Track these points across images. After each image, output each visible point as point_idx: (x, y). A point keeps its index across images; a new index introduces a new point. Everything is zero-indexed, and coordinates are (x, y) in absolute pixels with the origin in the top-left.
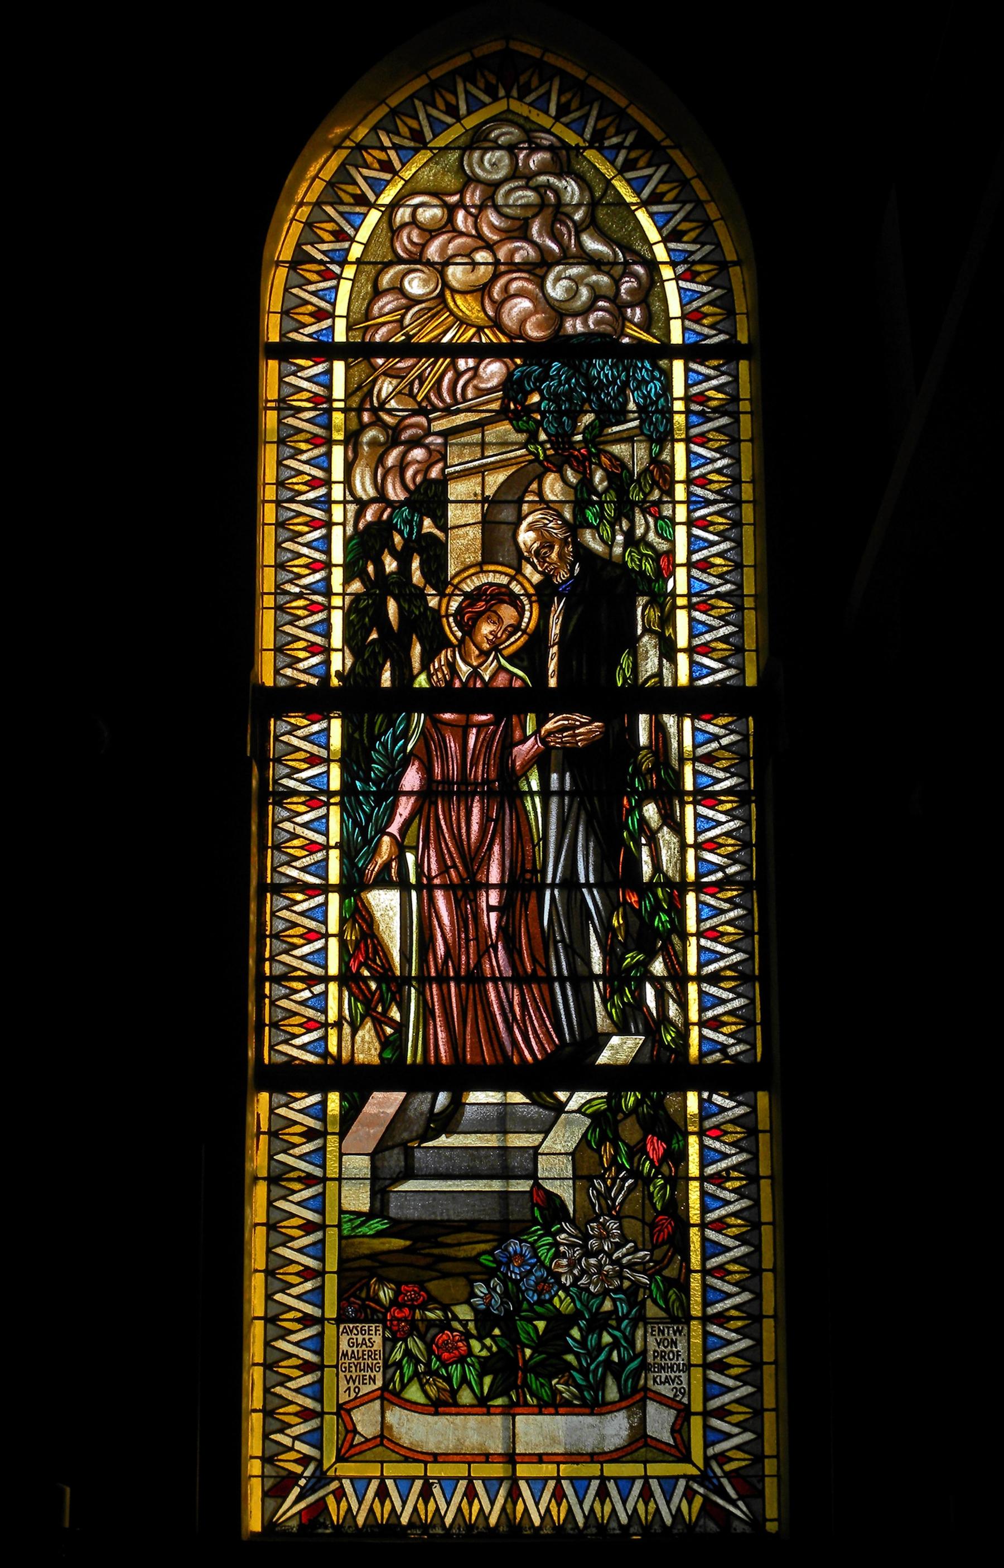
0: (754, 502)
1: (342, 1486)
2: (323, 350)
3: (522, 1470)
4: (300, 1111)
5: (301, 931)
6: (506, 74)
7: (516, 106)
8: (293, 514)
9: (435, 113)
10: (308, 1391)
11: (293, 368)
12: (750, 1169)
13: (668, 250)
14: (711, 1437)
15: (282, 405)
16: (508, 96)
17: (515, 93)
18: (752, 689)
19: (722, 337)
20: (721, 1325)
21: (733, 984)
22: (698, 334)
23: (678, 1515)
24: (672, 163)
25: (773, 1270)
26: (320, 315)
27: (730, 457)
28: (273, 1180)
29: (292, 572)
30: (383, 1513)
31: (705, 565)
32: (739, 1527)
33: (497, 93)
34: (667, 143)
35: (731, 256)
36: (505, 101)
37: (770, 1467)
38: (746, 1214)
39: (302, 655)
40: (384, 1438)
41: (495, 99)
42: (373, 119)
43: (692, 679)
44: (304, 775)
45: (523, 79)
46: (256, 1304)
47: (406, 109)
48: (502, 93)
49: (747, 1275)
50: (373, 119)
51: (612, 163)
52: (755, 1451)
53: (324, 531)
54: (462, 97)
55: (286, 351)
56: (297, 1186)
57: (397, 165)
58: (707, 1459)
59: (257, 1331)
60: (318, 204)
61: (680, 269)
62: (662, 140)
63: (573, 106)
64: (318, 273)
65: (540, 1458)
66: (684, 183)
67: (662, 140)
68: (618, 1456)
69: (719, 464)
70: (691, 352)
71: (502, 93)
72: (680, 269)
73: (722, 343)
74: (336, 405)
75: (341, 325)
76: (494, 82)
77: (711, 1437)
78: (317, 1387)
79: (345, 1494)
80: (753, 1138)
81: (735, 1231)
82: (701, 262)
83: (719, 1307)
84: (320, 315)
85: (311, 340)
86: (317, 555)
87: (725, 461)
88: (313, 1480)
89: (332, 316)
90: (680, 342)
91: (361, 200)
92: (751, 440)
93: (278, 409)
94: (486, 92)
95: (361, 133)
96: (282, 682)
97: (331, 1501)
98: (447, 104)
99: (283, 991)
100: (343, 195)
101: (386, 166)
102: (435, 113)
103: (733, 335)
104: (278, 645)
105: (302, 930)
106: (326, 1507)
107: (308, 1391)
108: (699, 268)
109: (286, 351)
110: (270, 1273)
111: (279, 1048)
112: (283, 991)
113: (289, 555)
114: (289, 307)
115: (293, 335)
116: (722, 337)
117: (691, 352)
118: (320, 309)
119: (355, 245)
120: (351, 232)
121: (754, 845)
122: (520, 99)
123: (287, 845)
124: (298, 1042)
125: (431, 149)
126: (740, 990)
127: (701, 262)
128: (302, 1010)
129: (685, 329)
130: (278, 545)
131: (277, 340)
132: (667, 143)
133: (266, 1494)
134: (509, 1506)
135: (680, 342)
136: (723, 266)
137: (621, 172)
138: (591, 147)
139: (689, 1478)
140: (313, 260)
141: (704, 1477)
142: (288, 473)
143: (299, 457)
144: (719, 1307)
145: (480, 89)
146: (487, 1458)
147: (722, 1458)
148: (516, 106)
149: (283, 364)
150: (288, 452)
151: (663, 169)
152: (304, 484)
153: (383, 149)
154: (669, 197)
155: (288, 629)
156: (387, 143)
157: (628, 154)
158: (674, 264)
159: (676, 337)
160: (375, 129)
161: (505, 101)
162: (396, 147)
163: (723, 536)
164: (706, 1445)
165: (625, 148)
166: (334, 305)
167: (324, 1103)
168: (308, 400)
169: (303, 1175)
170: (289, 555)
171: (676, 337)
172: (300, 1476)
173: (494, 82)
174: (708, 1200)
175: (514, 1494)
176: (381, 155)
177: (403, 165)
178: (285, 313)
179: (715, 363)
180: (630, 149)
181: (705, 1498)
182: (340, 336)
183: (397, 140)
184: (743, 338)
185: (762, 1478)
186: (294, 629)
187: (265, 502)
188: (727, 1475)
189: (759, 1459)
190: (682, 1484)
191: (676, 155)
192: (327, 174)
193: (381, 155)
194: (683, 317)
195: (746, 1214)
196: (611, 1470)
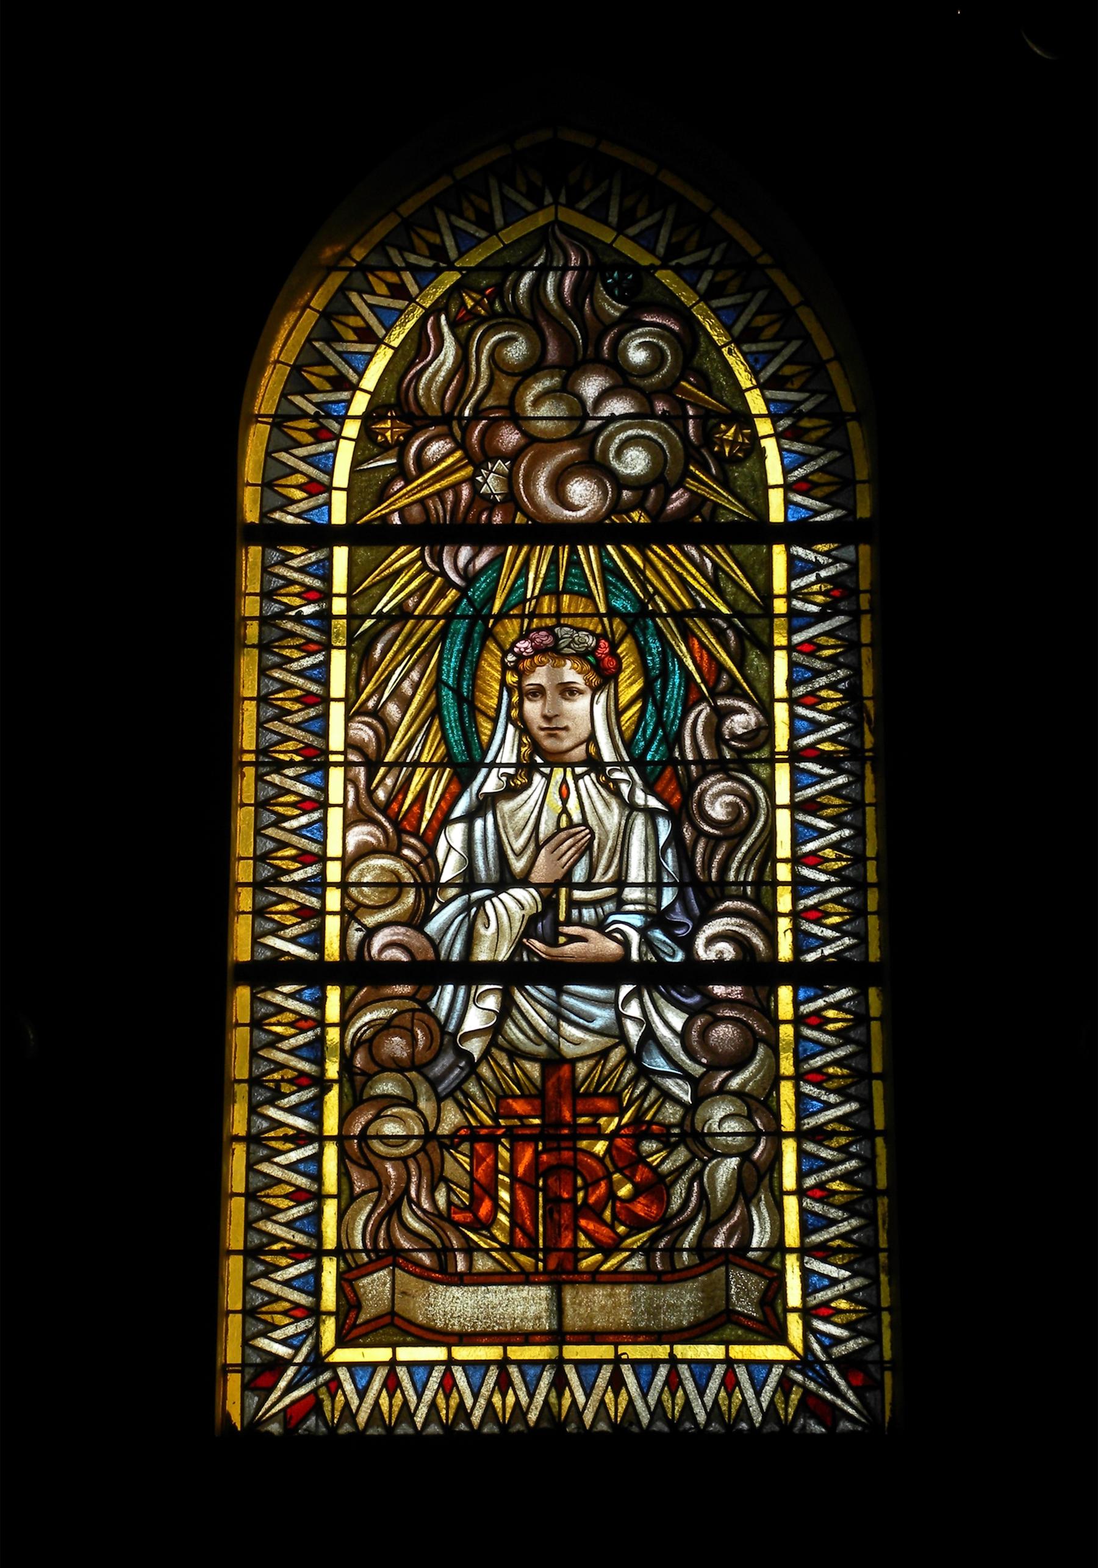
1: (336, 1378)
2: (321, 536)
3: (573, 1352)
5: (289, 1017)
7: (568, 216)
9: (460, 223)
10: (304, 1110)
11: (261, 1327)
13: (767, 402)
15: (261, 759)
16: (556, 203)
17: (563, 199)
19: (837, 513)
24: (773, 288)
27: (864, 1275)
29: (273, 920)
31: (812, 647)
32: (845, 1426)
34: (765, 259)
35: (848, 406)
36: (552, 209)
41: (540, 206)
42: (380, 232)
43: (798, 949)
44: (294, 824)
46: (235, 1236)
47: (425, 219)
48: (548, 199)
50: (380, 232)
51: (693, 287)
53: (310, 1206)
54: (496, 202)
55: (272, 535)
56: (283, 1261)
57: (413, 289)
59: (236, 1207)
61: (785, 423)
62: (759, 256)
63: (640, 213)
64: (310, 432)
67: (759, 256)
68: (695, 1334)
71: (548, 199)
72: (785, 423)
73: (835, 520)
74: (333, 758)
75: (339, 501)
76: (539, 183)
82: (811, 414)
85: (301, 521)
87: (858, 1282)
90: (781, 519)
91: (366, 335)
93: (256, 764)
94: (528, 196)
96: (263, 955)
97: (324, 1395)
98: (478, 211)
99: (261, 1268)
101: (398, 291)
102: (460, 223)
103: (852, 511)
104: (262, 745)
105: (290, 1017)
107: (304, 1053)
108: (805, 423)
109: (272, 535)
110: (250, 1196)
111: (260, 1167)
112: (261, 1268)
114: (273, 477)
115: (277, 515)
116: (837, 513)
117: (795, 533)
118: (312, 480)
122: (571, 205)
123: (277, 748)
124: (295, 666)
125: (460, 270)
127: (811, 414)
128: (294, 839)
129: (787, 502)
130: (260, 725)
132: (765, 259)
133: (245, 1387)
134: (553, 1399)
135: (781, 519)
136: (837, 419)
137: (705, 297)
138: (664, 266)
139: (788, 1364)
140: (305, 415)
142: (264, 1067)
143: (290, 563)
145: (521, 193)
146: (526, 1338)
148: (568, 216)
149: (268, 551)
151: (761, 295)
153: (397, 270)
154: (769, 333)
155: (276, 725)
156: (399, 262)
157: (713, 277)
158: (774, 418)
159: (776, 514)
161: (552, 209)
162: (414, 269)
165: (711, 267)
166: (331, 474)
168: (296, 752)
169: (291, 1132)
170: (275, 738)
172: (289, 1362)
173: (539, 183)
175: (560, 1383)
176: (392, 278)
177: (421, 289)
178: (261, 805)
180: (717, 268)
182: (339, 517)
183: (413, 259)
184: (864, 511)
186: (281, 833)
188: (838, 1362)
190: (777, 1371)
191: (778, 277)
193: (392, 278)
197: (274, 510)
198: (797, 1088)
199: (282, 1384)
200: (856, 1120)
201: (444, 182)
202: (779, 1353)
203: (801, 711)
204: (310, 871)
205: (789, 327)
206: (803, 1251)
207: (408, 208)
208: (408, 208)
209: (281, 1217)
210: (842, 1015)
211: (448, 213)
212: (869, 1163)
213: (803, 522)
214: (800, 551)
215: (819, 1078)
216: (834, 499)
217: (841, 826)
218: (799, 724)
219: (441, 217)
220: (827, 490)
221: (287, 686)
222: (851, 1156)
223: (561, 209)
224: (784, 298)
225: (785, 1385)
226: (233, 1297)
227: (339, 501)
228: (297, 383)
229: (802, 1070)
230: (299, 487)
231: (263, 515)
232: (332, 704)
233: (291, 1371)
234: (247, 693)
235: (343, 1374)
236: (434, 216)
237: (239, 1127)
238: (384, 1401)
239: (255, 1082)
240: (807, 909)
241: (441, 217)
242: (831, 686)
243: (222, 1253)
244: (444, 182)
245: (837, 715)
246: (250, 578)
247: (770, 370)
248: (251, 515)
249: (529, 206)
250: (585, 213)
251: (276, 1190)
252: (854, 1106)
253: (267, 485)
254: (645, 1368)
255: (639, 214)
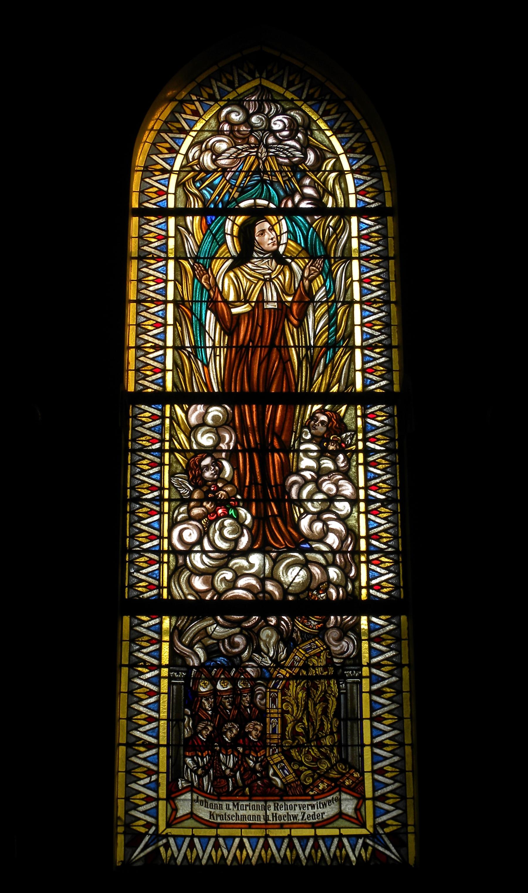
0: (412, 771)
1: (168, 841)
2: (163, 212)
4: (162, 159)
6: (261, 65)
7: (266, 83)
8: (139, 482)
12: (385, 298)
14: (375, 733)
17: (264, 75)
18: (396, 393)
19: (376, 204)
20: (378, 643)
21: (384, 454)
22: (366, 202)
23: (359, 858)
25: (409, 665)
26: (160, 193)
27: (395, 650)
28: (129, 745)
29: (141, 420)
30: (192, 857)
31: (368, 237)
33: (255, 75)
37: (411, 829)
38: (391, 531)
39: (152, 283)
40: (192, 815)
41: (254, 78)
42: (190, 88)
43: (364, 386)
45: (269, 68)
48: (257, 75)
49: (398, 800)
50: (190, 88)
52: (401, 819)
55: (142, 212)
57: (201, 112)
58: (375, 826)
60: (159, 131)
65: (282, 826)
66: (356, 122)
69: (384, 478)
70: (362, 212)
71: (257, 75)
75: (171, 198)
77: (375, 733)
78: (154, 811)
79: (170, 846)
80: (402, 748)
81: (379, 373)
83: (379, 712)
84: (160, 193)
86: (161, 276)
88: (154, 836)
89: (167, 193)
91: (182, 131)
92: (413, 798)
95: (184, 94)
97: (162, 849)
100: (174, 128)
101: (196, 113)
103: (384, 203)
106: (159, 851)
109: (142, 212)
111: (133, 706)
113: (142, 342)
119: (179, 155)
120: (177, 148)
121: (397, 440)
122: (267, 79)
126: (385, 353)
129: (357, 199)
131: (137, 206)
133: (126, 845)
141: (374, 836)
144: (379, 712)
147: (384, 825)
148: (266, 83)
150: (142, 308)
152: (152, 325)
160: (189, 93)
163: (379, 287)
164: (375, 817)
167: (161, 623)
170: (142, 342)
171: (354, 220)
174: (374, 705)
179: (373, 218)
181: (373, 847)
182: (171, 205)
184: (389, 204)
185: (407, 833)
187: (130, 325)
189: (405, 825)
190: (361, 841)
192: (164, 117)
194: (356, 193)
195: (385, 365)
196: (321, 832)
197: (144, 202)
198: (368, 567)
199: (142, 846)
200: (381, 253)
201: (215, 68)
202: (363, 831)
203: (363, 241)
204: (156, 494)
205: (356, 129)
206: (370, 665)
207: (199, 79)
208: (199, 79)
209: (141, 756)
210: (383, 414)
211: (216, 81)
212: (389, 314)
213: (363, 208)
214: (374, 619)
215: (370, 325)
216: (396, 778)
217: (379, 245)
218: (361, 225)
219: (214, 82)
220: (373, 194)
221: (150, 232)
222: (382, 311)
223: (263, 80)
224: (354, 116)
225: (365, 846)
226: (121, 766)
227: (171, 198)
228: (154, 149)
229: (369, 485)
230: (153, 281)
231: (140, 204)
232: (163, 643)
233: (147, 838)
234: (124, 662)
235: (171, 840)
236: (210, 82)
237: (132, 343)
238: (189, 853)
239: (138, 348)
240: (364, 235)
241: (214, 82)
242: (384, 482)
243: (128, 258)
244: (215, 68)
245: (379, 287)
246: (134, 231)
247: (349, 145)
248: (135, 204)
249: (249, 78)
250: (273, 82)
251: (138, 796)
252: (384, 314)
253: (142, 192)
254: (304, 840)
255: (296, 83)
